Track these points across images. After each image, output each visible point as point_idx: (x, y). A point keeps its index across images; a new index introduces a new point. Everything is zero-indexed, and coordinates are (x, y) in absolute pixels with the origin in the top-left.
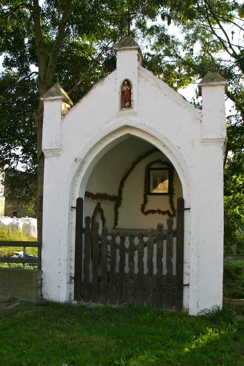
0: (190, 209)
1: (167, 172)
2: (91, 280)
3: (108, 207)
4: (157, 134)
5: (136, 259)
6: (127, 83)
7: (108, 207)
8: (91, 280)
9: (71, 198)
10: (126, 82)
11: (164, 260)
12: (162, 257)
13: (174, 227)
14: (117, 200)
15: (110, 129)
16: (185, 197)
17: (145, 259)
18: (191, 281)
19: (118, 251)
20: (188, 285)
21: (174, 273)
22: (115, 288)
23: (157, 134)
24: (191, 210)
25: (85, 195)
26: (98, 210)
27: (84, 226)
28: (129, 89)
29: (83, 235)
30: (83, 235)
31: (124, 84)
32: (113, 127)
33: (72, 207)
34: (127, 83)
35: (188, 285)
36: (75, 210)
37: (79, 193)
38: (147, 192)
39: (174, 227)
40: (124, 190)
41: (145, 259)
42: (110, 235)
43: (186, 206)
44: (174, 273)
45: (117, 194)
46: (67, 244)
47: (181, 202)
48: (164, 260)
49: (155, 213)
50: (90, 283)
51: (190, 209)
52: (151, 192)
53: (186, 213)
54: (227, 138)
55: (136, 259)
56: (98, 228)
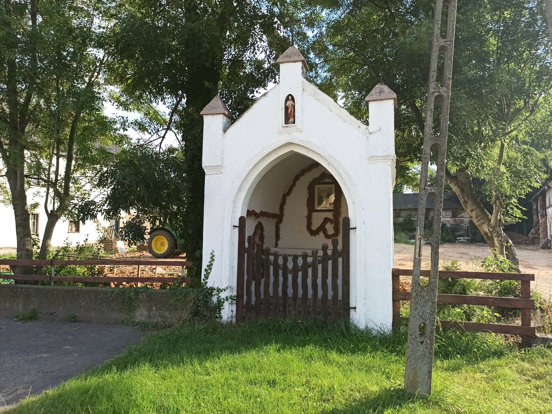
0: (355, 228)
1: (333, 186)
2: (253, 302)
3: (269, 226)
4: (321, 152)
5: (300, 280)
6: (290, 98)
7: (269, 226)
8: (253, 302)
9: (233, 218)
10: (290, 97)
11: (329, 281)
12: (327, 278)
13: (340, 247)
14: (279, 218)
15: (274, 146)
16: (351, 216)
17: (309, 281)
18: (358, 304)
19: (281, 272)
20: (355, 308)
21: (340, 297)
22: (278, 311)
23: (321, 152)
24: (357, 230)
25: (247, 215)
26: (259, 227)
27: (247, 245)
28: (293, 104)
29: (246, 254)
30: (246, 254)
31: (287, 99)
32: (276, 144)
33: (234, 226)
34: (290, 98)
35: (355, 308)
36: (237, 229)
37: (240, 212)
38: (311, 209)
39: (340, 247)
40: (285, 207)
41: (309, 281)
42: (272, 254)
43: (352, 226)
44: (340, 297)
45: (277, 212)
46: (229, 264)
47: (347, 221)
48: (329, 281)
49: (308, 172)
50: (252, 305)
51: (355, 228)
52: (315, 209)
53: (352, 232)
54: (395, 156)
55: (300, 280)
56: (541, 206)
